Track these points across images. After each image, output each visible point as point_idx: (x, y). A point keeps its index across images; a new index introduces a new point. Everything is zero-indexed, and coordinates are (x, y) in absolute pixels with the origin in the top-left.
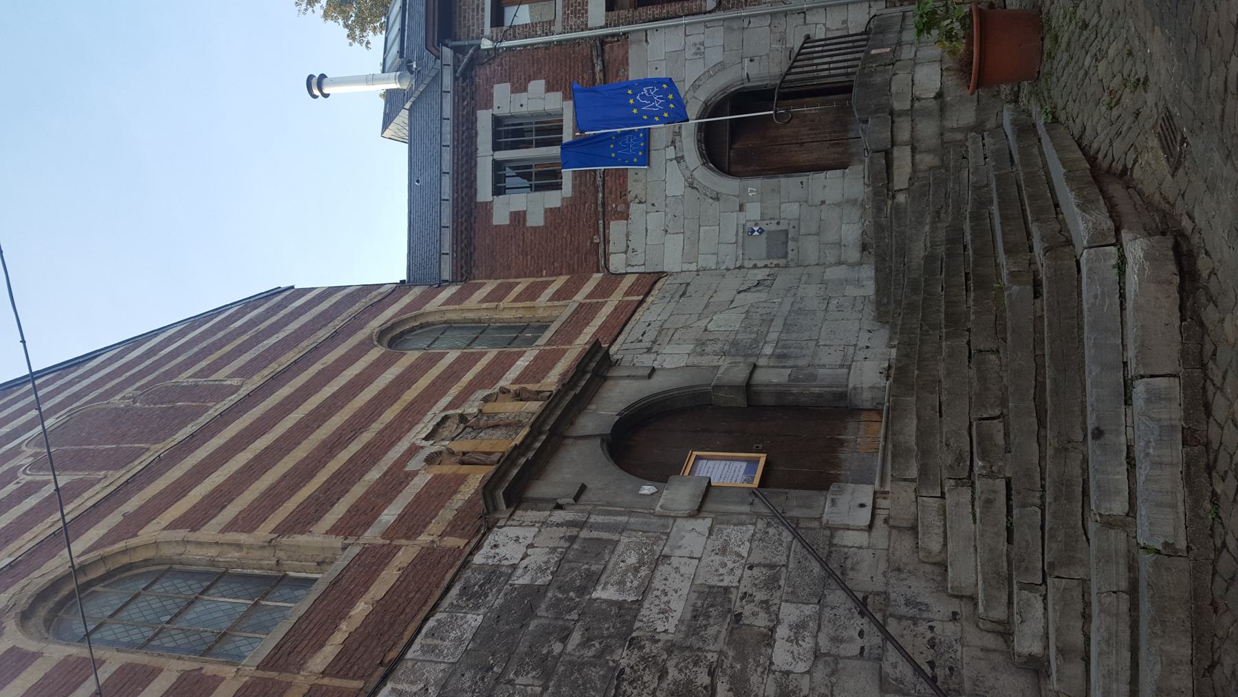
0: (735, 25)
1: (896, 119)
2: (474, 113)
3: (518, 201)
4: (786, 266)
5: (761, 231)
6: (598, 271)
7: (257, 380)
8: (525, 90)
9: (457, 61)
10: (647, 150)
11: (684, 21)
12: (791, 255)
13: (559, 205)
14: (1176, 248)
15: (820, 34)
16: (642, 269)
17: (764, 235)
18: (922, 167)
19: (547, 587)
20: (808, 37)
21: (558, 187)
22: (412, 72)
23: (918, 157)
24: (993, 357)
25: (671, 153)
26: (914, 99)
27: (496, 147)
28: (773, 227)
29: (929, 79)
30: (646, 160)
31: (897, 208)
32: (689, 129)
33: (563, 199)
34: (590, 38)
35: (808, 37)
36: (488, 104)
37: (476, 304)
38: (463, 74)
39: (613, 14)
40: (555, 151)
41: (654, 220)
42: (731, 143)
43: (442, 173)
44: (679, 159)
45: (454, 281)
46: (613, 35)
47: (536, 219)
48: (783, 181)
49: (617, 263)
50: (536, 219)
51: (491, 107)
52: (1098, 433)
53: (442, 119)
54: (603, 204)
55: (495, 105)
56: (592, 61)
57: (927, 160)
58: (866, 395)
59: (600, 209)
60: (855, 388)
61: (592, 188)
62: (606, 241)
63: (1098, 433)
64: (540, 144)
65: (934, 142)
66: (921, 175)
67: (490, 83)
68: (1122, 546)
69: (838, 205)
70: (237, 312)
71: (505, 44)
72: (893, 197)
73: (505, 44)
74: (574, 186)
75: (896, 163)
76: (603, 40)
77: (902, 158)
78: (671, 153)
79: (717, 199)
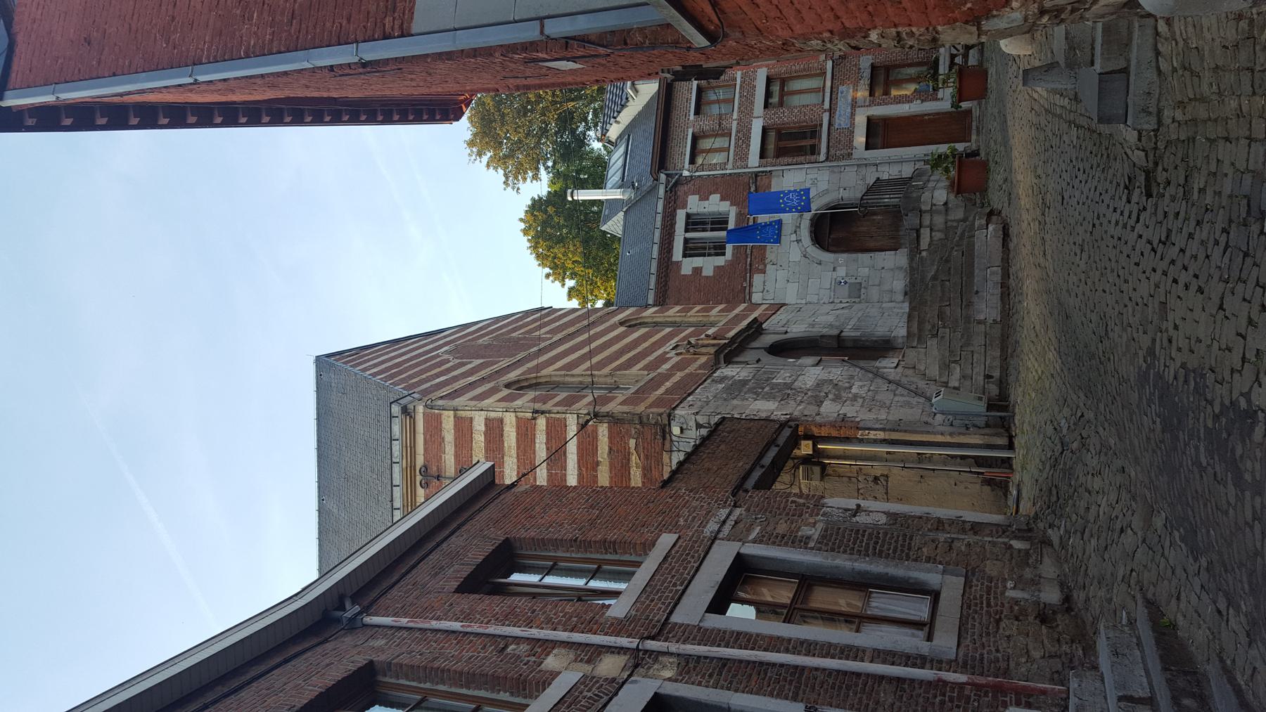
0: (836, 170)
1: (923, 215)
2: (675, 210)
3: (698, 262)
4: (860, 302)
5: (846, 283)
6: (745, 303)
7: (559, 336)
8: (708, 199)
9: (668, 182)
10: (779, 235)
11: (806, 166)
12: (863, 297)
13: (723, 264)
14: (1004, 228)
15: (885, 177)
16: (772, 302)
17: (847, 285)
18: (935, 239)
19: (750, 380)
20: (878, 179)
21: (724, 254)
22: (634, 188)
23: (933, 234)
24: (947, 283)
25: (794, 237)
26: (933, 205)
27: (687, 231)
28: (853, 280)
29: (941, 196)
30: (778, 241)
31: (921, 258)
32: (808, 216)
33: (726, 261)
34: (749, 172)
35: (878, 179)
36: (684, 206)
37: (673, 312)
38: (671, 190)
39: (764, 161)
40: (724, 233)
41: (781, 275)
42: (830, 234)
43: (654, 243)
44: (798, 241)
45: (654, 305)
46: (763, 172)
47: (708, 272)
48: (860, 255)
49: (756, 298)
50: (708, 272)
51: (686, 208)
52: (977, 292)
53: (656, 213)
54: (751, 265)
55: (688, 208)
56: (749, 185)
57: (937, 235)
58: (900, 340)
59: (748, 267)
60: (894, 337)
61: (744, 256)
62: (751, 285)
63: (977, 292)
64: (712, 230)
65: (942, 226)
66: (935, 243)
67: (686, 194)
68: (983, 330)
69: (892, 270)
70: (523, 316)
71: (697, 174)
72: (920, 253)
73: (697, 174)
74: (733, 254)
75: (922, 236)
76: (756, 175)
77: (925, 233)
78: (794, 237)
79: (820, 264)
